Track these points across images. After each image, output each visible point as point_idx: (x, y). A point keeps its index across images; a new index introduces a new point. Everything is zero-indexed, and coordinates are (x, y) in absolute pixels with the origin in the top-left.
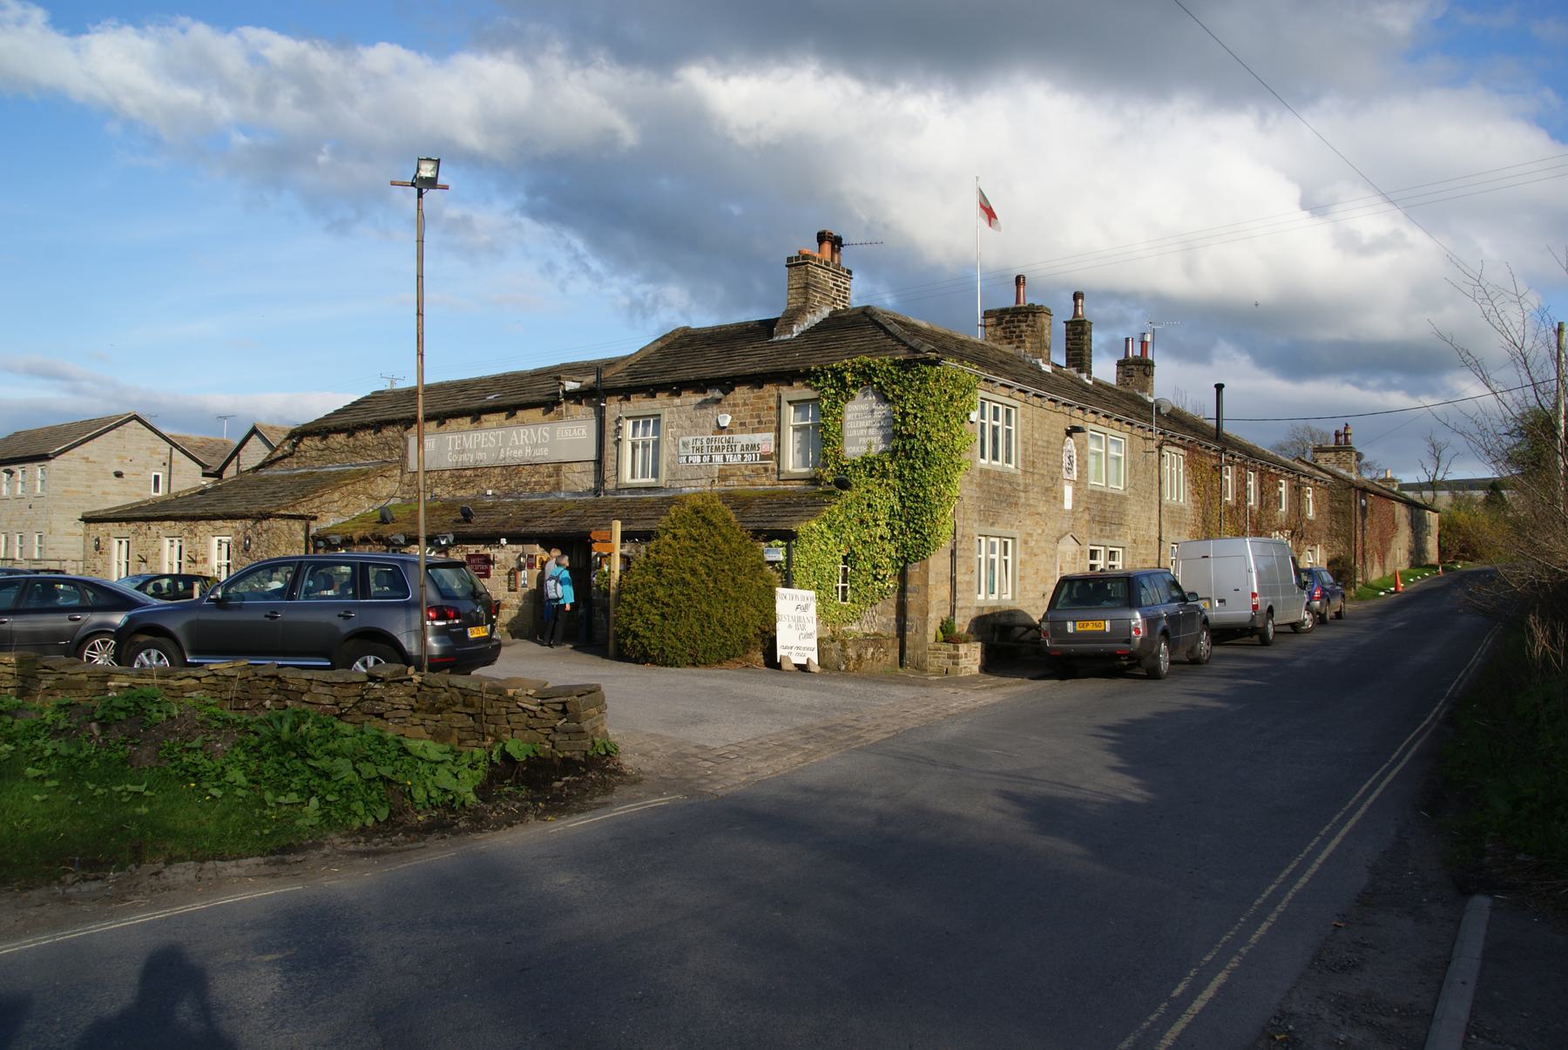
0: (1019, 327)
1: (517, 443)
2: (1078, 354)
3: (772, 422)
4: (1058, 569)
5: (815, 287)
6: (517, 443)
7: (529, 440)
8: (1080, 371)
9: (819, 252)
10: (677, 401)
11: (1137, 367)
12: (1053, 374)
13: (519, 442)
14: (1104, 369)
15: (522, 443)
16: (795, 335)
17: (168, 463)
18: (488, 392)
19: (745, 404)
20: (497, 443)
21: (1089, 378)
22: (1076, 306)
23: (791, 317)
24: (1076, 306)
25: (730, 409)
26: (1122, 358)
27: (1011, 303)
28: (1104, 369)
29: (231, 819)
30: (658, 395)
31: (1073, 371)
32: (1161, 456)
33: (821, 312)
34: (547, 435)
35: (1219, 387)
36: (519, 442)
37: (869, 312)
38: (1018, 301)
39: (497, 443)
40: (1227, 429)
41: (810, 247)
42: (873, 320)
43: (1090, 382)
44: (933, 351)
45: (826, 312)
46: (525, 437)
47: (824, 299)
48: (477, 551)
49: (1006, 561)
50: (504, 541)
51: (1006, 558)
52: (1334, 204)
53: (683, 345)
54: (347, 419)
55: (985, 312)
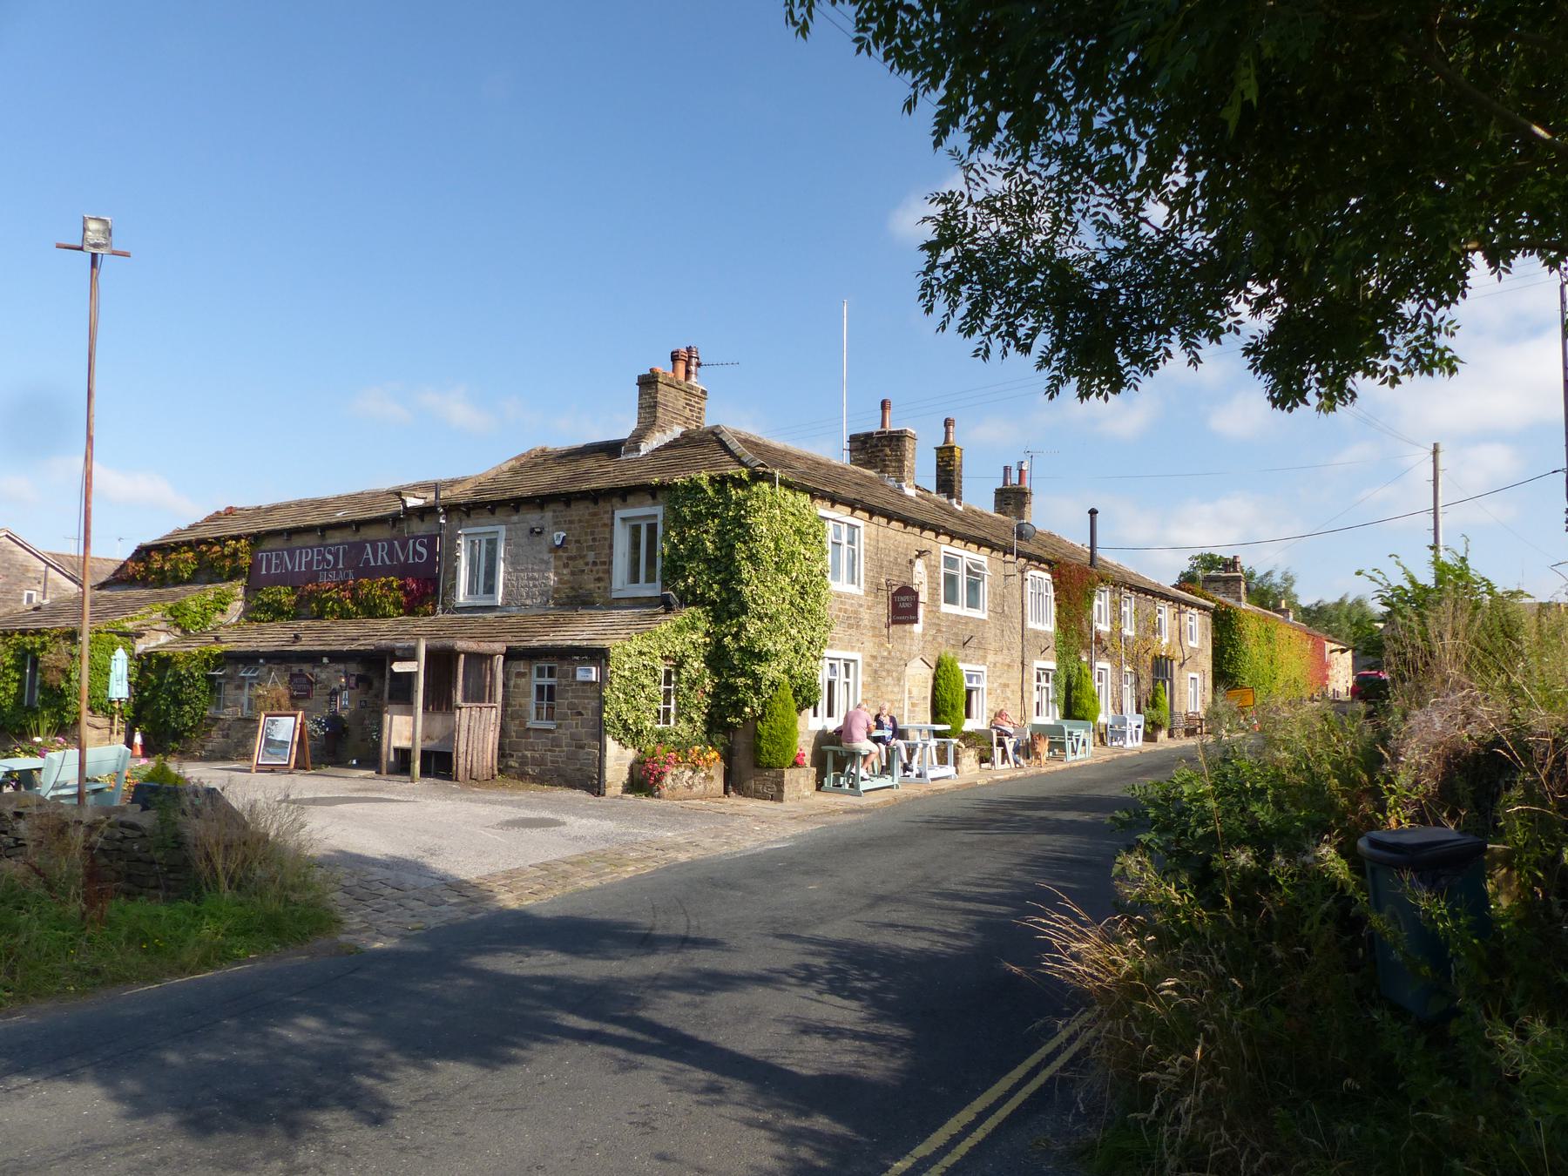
0: (882, 451)
1: (373, 564)
2: (947, 480)
3: (605, 539)
4: (907, 692)
5: (666, 406)
6: (373, 564)
7: (391, 560)
8: (950, 497)
9: (673, 371)
10: (515, 518)
11: (1012, 498)
12: (919, 500)
13: (376, 561)
14: (978, 495)
15: (379, 563)
16: (641, 454)
17: (43, 581)
18: (338, 509)
19: (580, 521)
20: (336, 562)
21: (959, 504)
22: (947, 433)
23: (638, 437)
24: (947, 433)
25: (566, 526)
26: (1000, 485)
27: (875, 428)
28: (978, 495)
29: (281, 910)
30: (497, 511)
31: (943, 499)
32: (1024, 580)
33: (672, 430)
34: (424, 551)
35: (1093, 512)
36: (376, 561)
37: (717, 431)
38: (883, 425)
39: (336, 562)
40: (1105, 555)
41: (664, 367)
42: (718, 438)
43: (960, 508)
44: (762, 465)
45: (677, 431)
46: (384, 553)
47: (676, 418)
48: (301, 670)
49: (847, 683)
50: (325, 660)
51: (847, 680)
52: (1418, 445)
53: (536, 465)
54: (191, 537)
55: (851, 437)
